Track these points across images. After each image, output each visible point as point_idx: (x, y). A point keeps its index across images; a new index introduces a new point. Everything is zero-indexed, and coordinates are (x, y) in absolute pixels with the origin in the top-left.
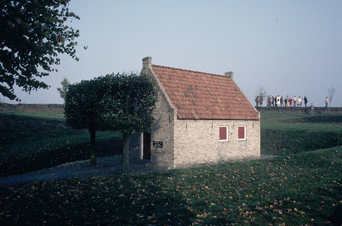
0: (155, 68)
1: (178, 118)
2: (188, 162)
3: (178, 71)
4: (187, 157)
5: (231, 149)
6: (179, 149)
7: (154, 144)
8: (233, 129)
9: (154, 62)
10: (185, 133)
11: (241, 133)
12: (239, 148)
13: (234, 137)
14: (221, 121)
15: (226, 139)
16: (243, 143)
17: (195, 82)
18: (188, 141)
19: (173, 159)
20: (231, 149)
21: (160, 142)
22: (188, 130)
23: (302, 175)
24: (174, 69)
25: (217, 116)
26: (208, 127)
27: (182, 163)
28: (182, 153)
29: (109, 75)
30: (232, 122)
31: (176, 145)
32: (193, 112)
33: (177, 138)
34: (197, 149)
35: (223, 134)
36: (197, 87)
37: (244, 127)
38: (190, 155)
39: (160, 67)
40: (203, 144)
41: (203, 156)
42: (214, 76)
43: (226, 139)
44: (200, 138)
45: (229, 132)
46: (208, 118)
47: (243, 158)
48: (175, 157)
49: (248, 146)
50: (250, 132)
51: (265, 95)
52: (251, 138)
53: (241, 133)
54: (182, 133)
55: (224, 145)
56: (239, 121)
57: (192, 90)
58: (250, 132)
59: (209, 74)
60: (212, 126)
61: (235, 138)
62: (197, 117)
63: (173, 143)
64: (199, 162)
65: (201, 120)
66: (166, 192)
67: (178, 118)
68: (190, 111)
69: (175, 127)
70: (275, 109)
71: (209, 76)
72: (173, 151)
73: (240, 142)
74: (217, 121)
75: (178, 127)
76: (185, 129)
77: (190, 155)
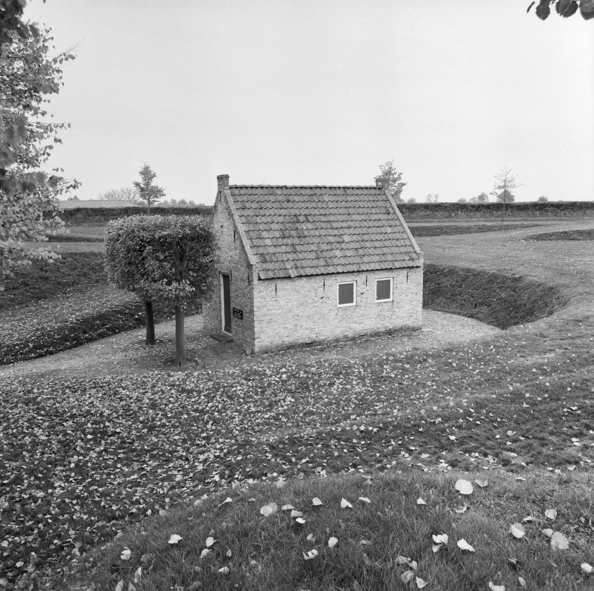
0: (236, 192)
1: (260, 279)
2: (280, 342)
3: (279, 192)
4: (279, 334)
5: (361, 318)
6: (264, 324)
7: (234, 311)
8: (365, 285)
9: (232, 182)
10: (274, 299)
11: (384, 290)
12: (377, 314)
13: (366, 298)
14: (341, 275)
15: (352, 301)
16: (386, 307)
17: (307, 208)
18: (280, 311)
19: (254, 339)
20: (361, 318)
21: (240, 311)
22: (278, 294)
23: (114, 396)
24: (272, 188)
25: (335, 268)
26: (316, 287)
27: (269, 343)
28: (268, 330)
29: (157, 187)
30: (363, 277)
31: (257, 318)
32: (288, 265)
33: (258, 308)
34: (296, 322)
35: (346, 294)
36: (308, 217)
37: (390, 280)
38: (282, 331)
39: (246, 188)
40: (307, 314)
41: (307, 332)
42: (348, 192)
43: (352, 301)
44: (302, 304)
45: (357, 291)
46: (315, 274)
47: (386, 331)
48: (256, 335)
49: (397, 310)
50: (401, 288)
51: (512, 183)
52: (403, 296)
53: (384, 290)
54: (268, 299)
55: (348, 312)
56: (377, 272)
57: (298, 225)
58: (401, 288)
59: (339, 188)
60: (324, 285)
61: (369, 300)
62: (293, 273)
63: (253, 315)
64: (301, 341)
65: (303, 278)
66: (494, 396)
67: (260, 279)
68: (284, 264)
69: (255, 292)
70: (537, 208)
71: (338, 192)
72: (254, 327)
73: (379, 306)
74: (333, 276)
75: (260, 291)
76: (274, 293)
77: (282, 331)
